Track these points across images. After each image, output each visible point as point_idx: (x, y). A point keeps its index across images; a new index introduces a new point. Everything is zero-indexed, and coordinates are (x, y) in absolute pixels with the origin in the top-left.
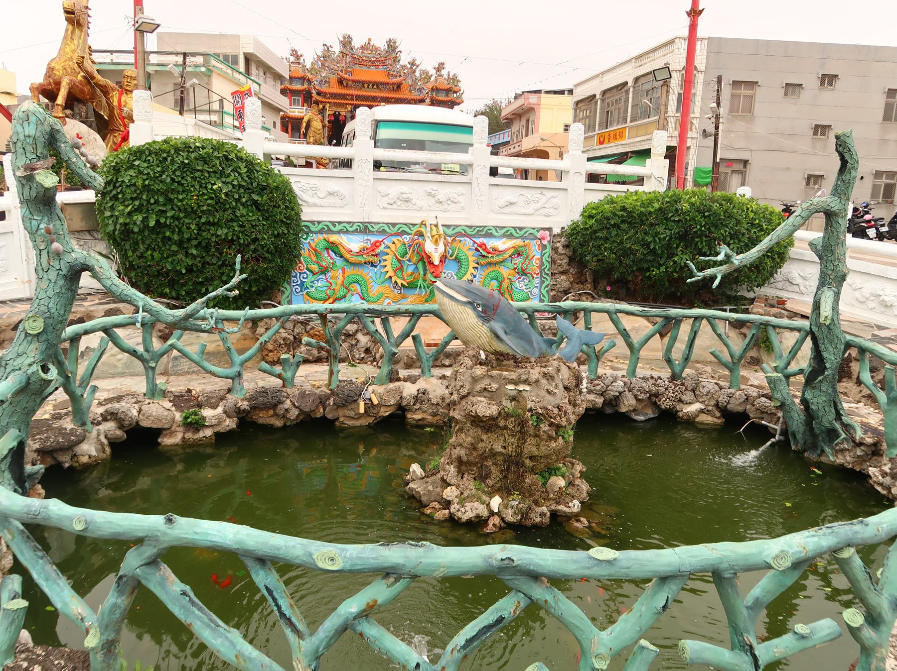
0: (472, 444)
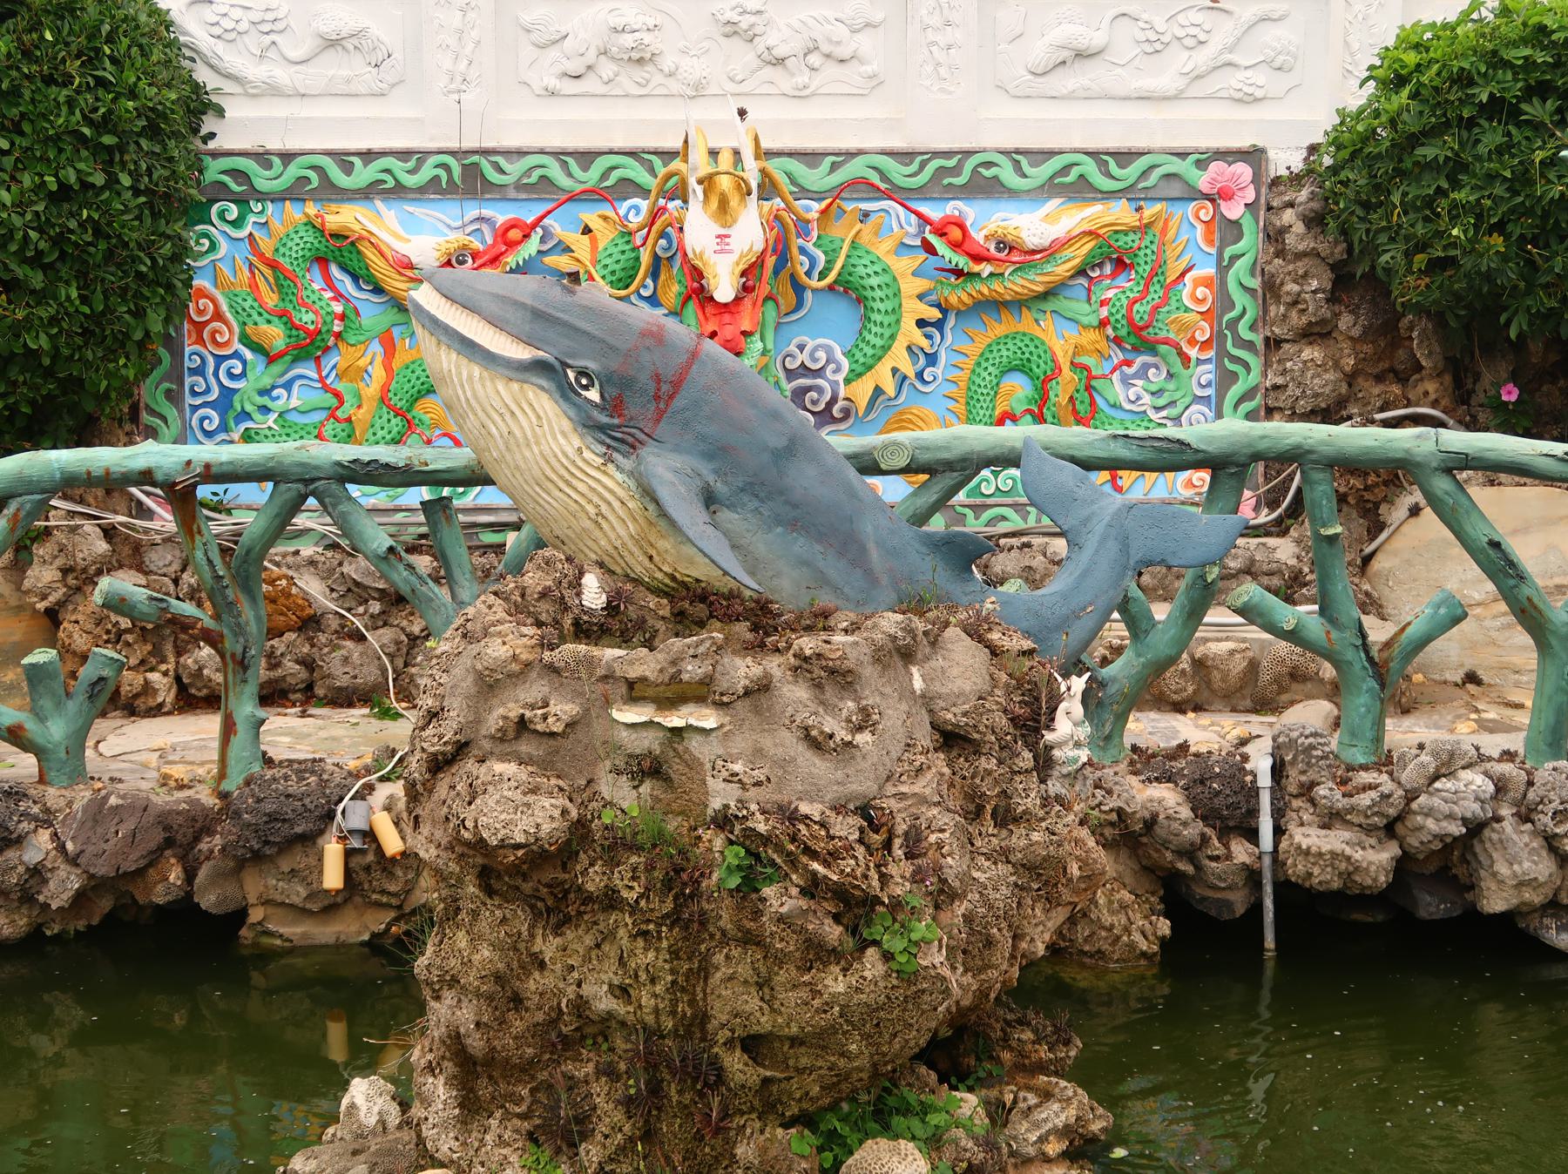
0: (499, 978)
